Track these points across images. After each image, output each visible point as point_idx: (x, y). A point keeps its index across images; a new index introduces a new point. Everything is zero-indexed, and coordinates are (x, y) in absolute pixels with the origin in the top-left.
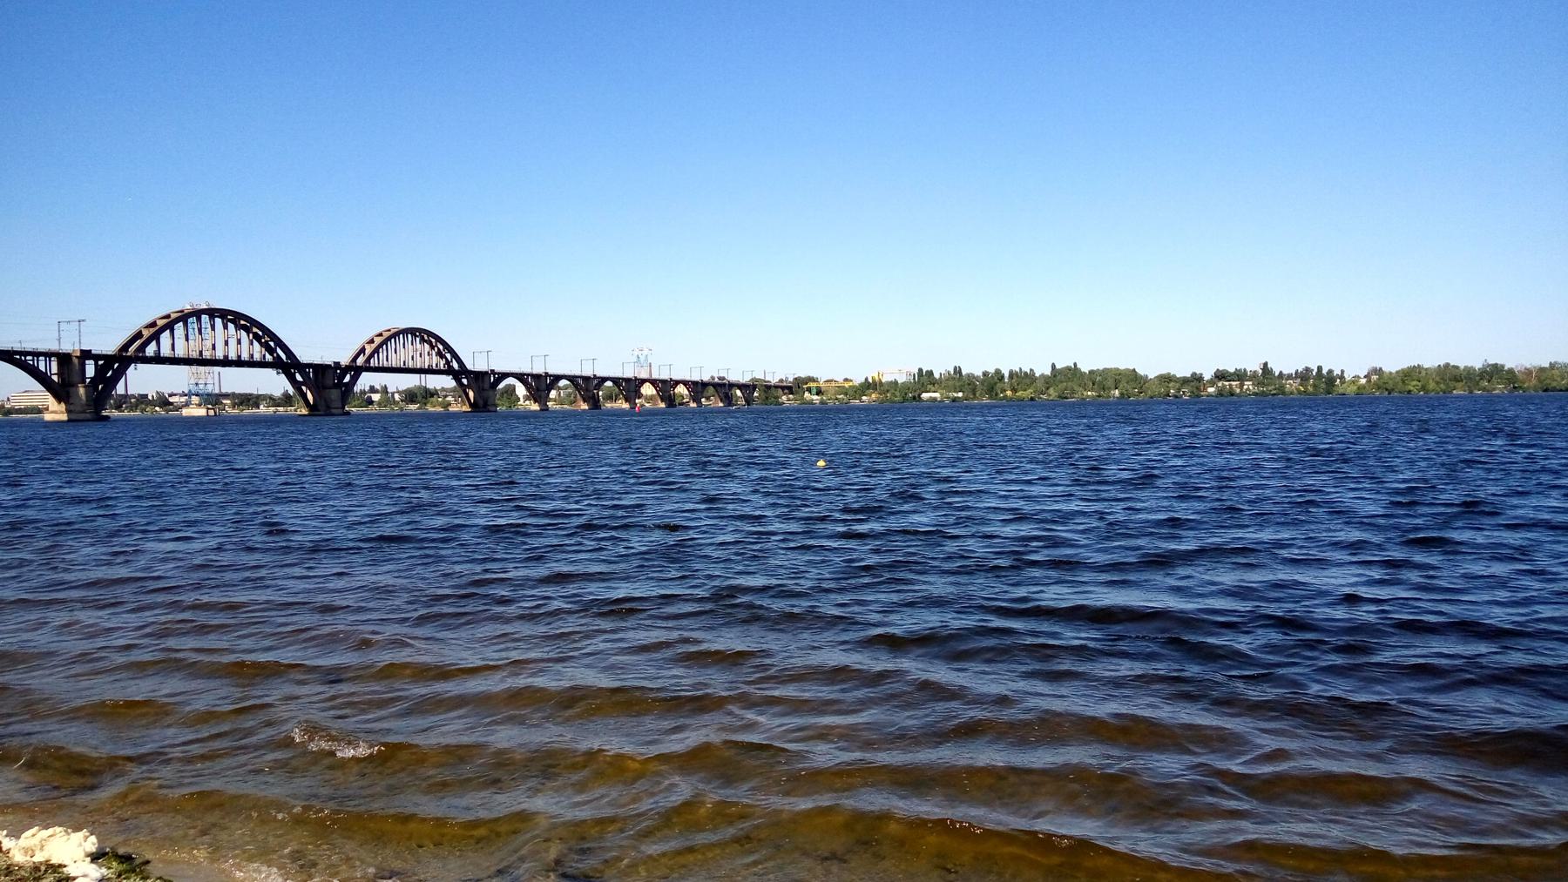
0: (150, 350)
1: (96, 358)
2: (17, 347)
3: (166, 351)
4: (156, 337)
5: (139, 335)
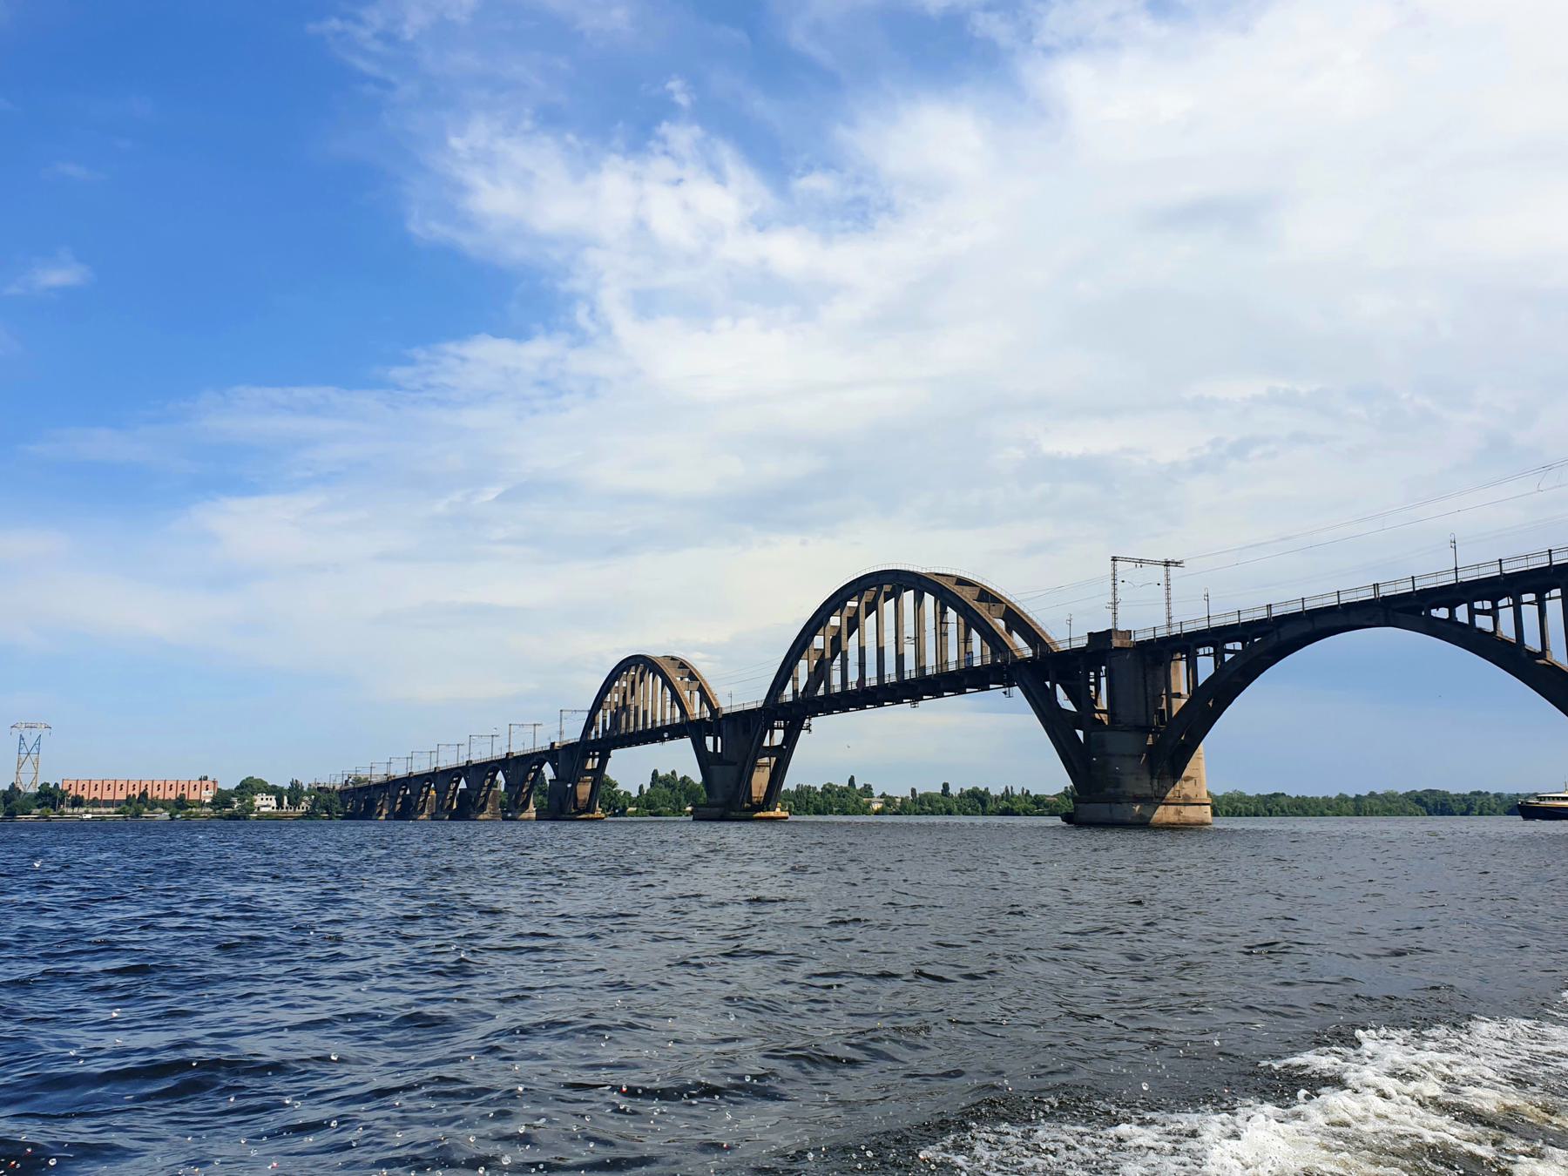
2: (1433, 571)
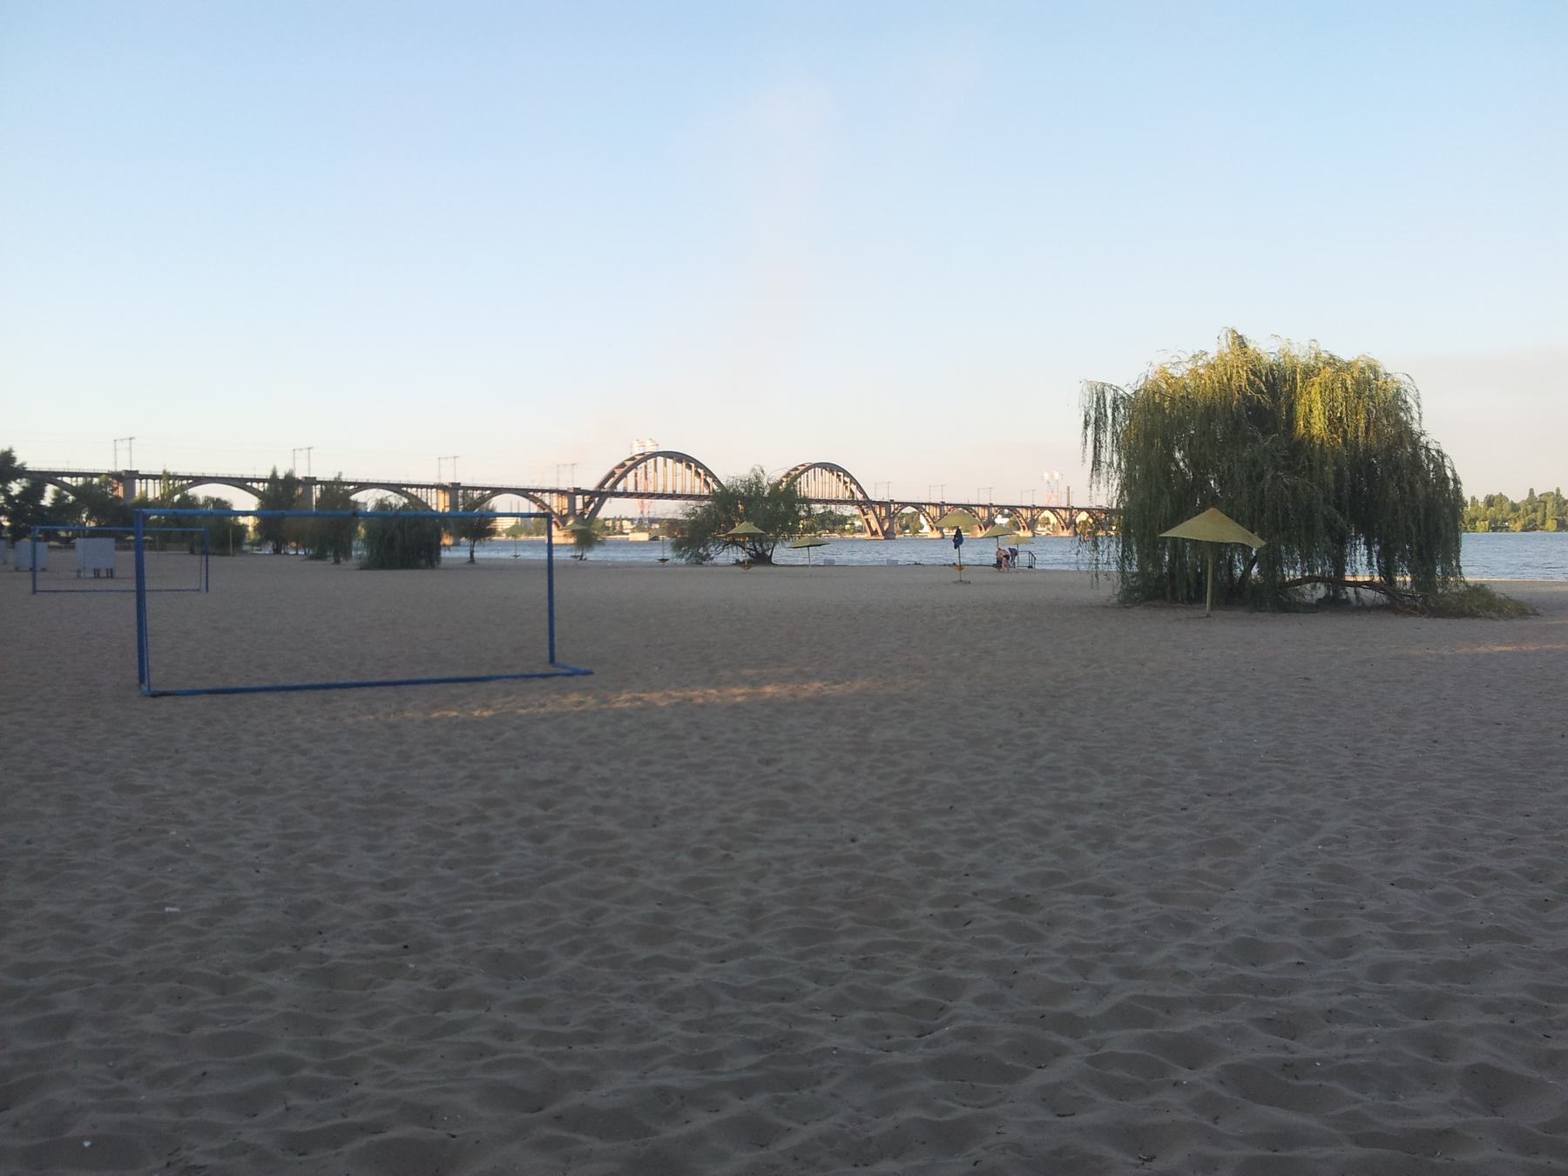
0: (620, 488)
1: (584, 493)
2: (248, 474)
3: (631, 489)
4: (624, 475)
5: (612, 474)
